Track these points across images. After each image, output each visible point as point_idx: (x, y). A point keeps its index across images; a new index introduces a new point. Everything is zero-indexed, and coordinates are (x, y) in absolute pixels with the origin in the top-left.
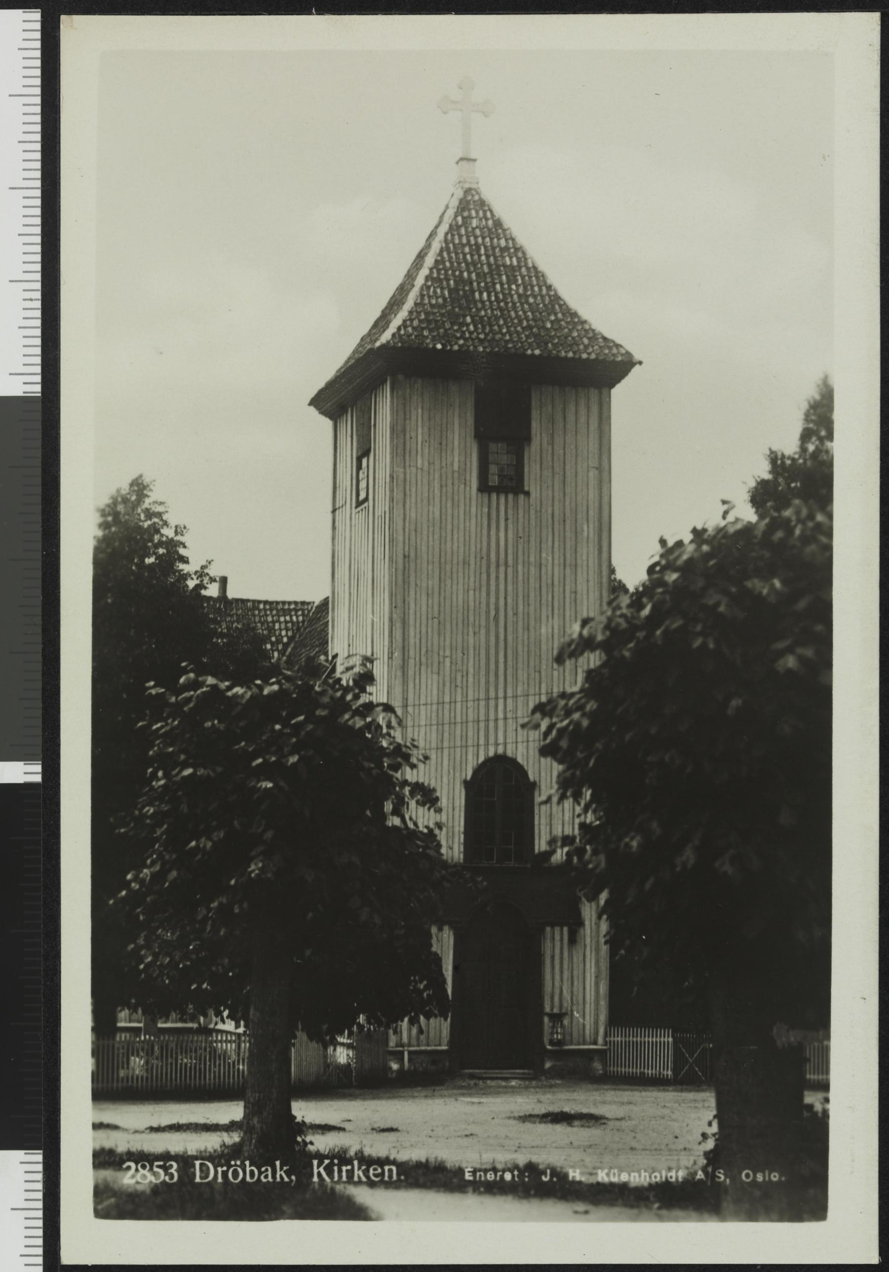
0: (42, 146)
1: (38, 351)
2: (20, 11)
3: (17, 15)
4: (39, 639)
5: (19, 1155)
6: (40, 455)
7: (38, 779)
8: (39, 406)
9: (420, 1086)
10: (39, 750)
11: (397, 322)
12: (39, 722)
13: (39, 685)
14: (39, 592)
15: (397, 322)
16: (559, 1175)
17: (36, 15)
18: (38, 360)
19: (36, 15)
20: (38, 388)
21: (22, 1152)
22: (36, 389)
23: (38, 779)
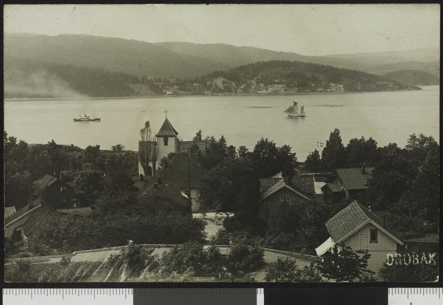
0: (49, 288)
1: (118, 289)
2: (3, 296)
3: (4, 297)
4: (215, 289)
5: (390, 296)
6: (153, 289)
7: (262, 289)
8: (137, 289)
9: (106, 245)
10: (253, 289)
11: (15, 99)
12: (243, 289)
13: (231, 289)
14: (199, 289)
15: (15, 99)
16: (81, 271)
17: (5, 290)
18: (121, 289)
19: (5, 290)
20: (131, 289)
21: (389, 295)
22: (131, 290)
23: (262, 289)
